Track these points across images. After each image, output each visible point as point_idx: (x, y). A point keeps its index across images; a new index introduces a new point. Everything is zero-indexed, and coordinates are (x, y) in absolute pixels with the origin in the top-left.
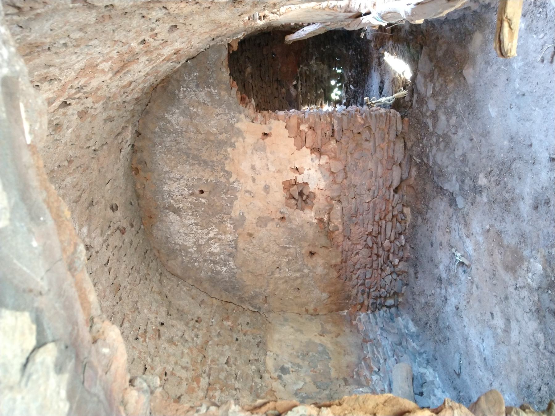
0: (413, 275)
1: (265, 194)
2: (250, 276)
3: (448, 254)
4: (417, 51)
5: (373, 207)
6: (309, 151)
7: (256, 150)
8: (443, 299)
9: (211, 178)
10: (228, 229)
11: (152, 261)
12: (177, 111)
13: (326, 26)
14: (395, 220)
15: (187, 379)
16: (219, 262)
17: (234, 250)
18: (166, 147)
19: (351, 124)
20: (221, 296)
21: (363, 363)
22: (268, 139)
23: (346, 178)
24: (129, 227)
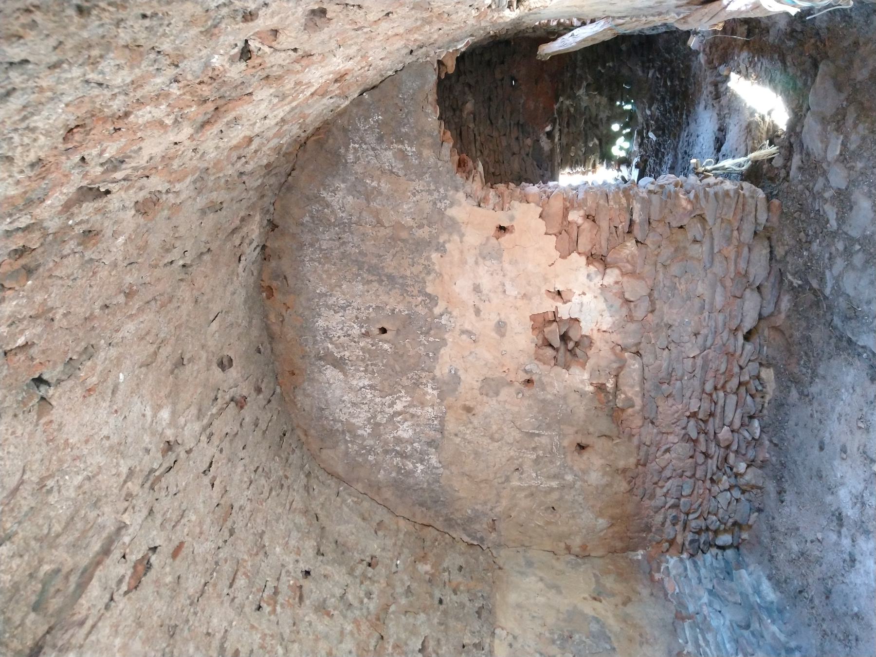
0: (773, 495)
1: (498, 337)
2: (466, 482)
3: (860, 472)
4: (804, 72)
5: (703, 368)
6: (583, 260)
7: (484, 258)
9: (401, 307)
10: (428, 397)
11: (293, 451)
12: (343, 186)
13: (617, 25)
14: (743, 390)
16: (411, 455)
17: (439, 436)
18: (321, 250)
19: (667, 211)
20: (414, 515)
22: (506, 238)
23: (652, 311)
24: (254, 394)
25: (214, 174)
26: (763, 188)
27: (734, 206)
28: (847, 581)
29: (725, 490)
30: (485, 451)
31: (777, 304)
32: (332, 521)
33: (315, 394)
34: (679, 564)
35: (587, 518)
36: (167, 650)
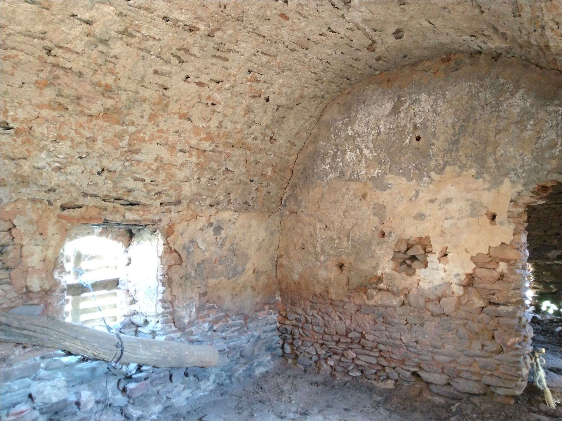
0: (315, 379)
1: (414, 215)
2: (318, 196)
6: (470, 271)
7: (471, 205)
8: (283, 414)
9: (435, 149)
10: (372, 170)
11: (338, 86)
12: (528, 104)
14: (379, 368)
15: (209, 127)
16: (334, 161)
17: (347, 178)
18: (478, 93)
19: (506, 328)
21: (223, 314)
22: (487, 220)
23: (432, 315)
24: (376, 56)
25: (546, 6)
26: (523, 394)
27: (509, 373)
28: (270, 413)
29: (317, 352)
30: (338, 207)
31: (438, 394)
32: (296, 114)
33: (375, 97)
34: (274, 321)
35: (298, 268)
36: (230, 17)
